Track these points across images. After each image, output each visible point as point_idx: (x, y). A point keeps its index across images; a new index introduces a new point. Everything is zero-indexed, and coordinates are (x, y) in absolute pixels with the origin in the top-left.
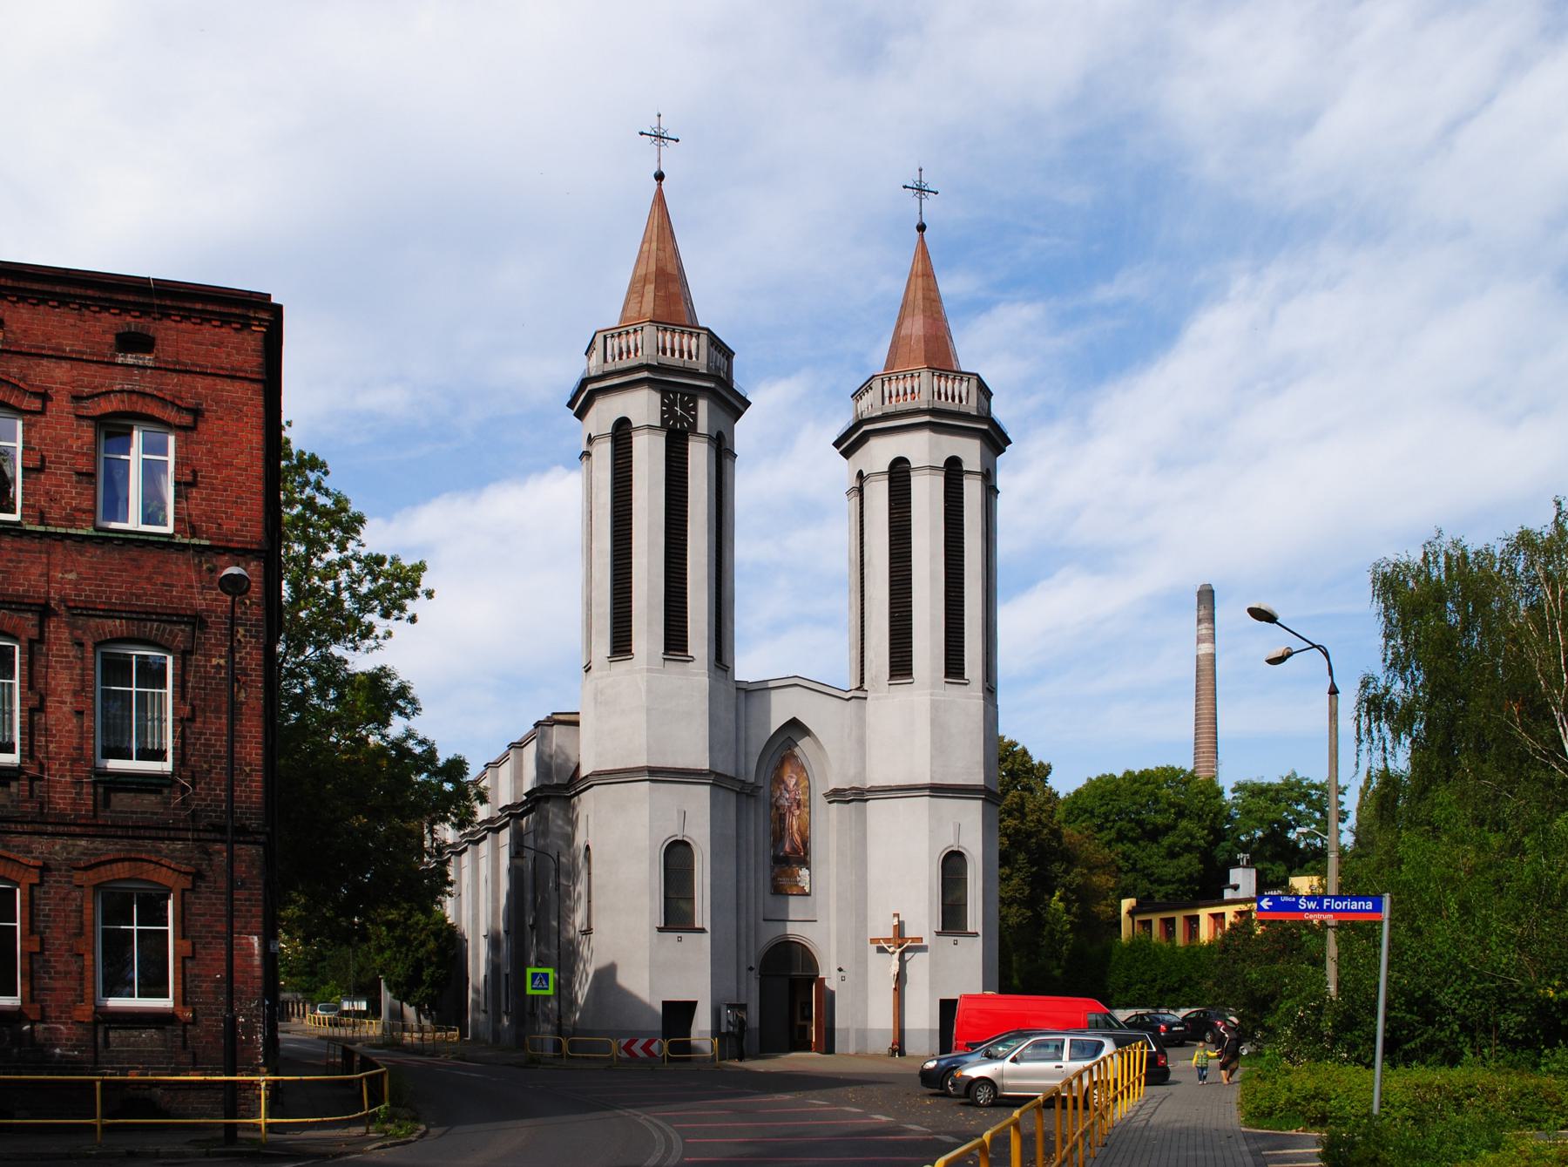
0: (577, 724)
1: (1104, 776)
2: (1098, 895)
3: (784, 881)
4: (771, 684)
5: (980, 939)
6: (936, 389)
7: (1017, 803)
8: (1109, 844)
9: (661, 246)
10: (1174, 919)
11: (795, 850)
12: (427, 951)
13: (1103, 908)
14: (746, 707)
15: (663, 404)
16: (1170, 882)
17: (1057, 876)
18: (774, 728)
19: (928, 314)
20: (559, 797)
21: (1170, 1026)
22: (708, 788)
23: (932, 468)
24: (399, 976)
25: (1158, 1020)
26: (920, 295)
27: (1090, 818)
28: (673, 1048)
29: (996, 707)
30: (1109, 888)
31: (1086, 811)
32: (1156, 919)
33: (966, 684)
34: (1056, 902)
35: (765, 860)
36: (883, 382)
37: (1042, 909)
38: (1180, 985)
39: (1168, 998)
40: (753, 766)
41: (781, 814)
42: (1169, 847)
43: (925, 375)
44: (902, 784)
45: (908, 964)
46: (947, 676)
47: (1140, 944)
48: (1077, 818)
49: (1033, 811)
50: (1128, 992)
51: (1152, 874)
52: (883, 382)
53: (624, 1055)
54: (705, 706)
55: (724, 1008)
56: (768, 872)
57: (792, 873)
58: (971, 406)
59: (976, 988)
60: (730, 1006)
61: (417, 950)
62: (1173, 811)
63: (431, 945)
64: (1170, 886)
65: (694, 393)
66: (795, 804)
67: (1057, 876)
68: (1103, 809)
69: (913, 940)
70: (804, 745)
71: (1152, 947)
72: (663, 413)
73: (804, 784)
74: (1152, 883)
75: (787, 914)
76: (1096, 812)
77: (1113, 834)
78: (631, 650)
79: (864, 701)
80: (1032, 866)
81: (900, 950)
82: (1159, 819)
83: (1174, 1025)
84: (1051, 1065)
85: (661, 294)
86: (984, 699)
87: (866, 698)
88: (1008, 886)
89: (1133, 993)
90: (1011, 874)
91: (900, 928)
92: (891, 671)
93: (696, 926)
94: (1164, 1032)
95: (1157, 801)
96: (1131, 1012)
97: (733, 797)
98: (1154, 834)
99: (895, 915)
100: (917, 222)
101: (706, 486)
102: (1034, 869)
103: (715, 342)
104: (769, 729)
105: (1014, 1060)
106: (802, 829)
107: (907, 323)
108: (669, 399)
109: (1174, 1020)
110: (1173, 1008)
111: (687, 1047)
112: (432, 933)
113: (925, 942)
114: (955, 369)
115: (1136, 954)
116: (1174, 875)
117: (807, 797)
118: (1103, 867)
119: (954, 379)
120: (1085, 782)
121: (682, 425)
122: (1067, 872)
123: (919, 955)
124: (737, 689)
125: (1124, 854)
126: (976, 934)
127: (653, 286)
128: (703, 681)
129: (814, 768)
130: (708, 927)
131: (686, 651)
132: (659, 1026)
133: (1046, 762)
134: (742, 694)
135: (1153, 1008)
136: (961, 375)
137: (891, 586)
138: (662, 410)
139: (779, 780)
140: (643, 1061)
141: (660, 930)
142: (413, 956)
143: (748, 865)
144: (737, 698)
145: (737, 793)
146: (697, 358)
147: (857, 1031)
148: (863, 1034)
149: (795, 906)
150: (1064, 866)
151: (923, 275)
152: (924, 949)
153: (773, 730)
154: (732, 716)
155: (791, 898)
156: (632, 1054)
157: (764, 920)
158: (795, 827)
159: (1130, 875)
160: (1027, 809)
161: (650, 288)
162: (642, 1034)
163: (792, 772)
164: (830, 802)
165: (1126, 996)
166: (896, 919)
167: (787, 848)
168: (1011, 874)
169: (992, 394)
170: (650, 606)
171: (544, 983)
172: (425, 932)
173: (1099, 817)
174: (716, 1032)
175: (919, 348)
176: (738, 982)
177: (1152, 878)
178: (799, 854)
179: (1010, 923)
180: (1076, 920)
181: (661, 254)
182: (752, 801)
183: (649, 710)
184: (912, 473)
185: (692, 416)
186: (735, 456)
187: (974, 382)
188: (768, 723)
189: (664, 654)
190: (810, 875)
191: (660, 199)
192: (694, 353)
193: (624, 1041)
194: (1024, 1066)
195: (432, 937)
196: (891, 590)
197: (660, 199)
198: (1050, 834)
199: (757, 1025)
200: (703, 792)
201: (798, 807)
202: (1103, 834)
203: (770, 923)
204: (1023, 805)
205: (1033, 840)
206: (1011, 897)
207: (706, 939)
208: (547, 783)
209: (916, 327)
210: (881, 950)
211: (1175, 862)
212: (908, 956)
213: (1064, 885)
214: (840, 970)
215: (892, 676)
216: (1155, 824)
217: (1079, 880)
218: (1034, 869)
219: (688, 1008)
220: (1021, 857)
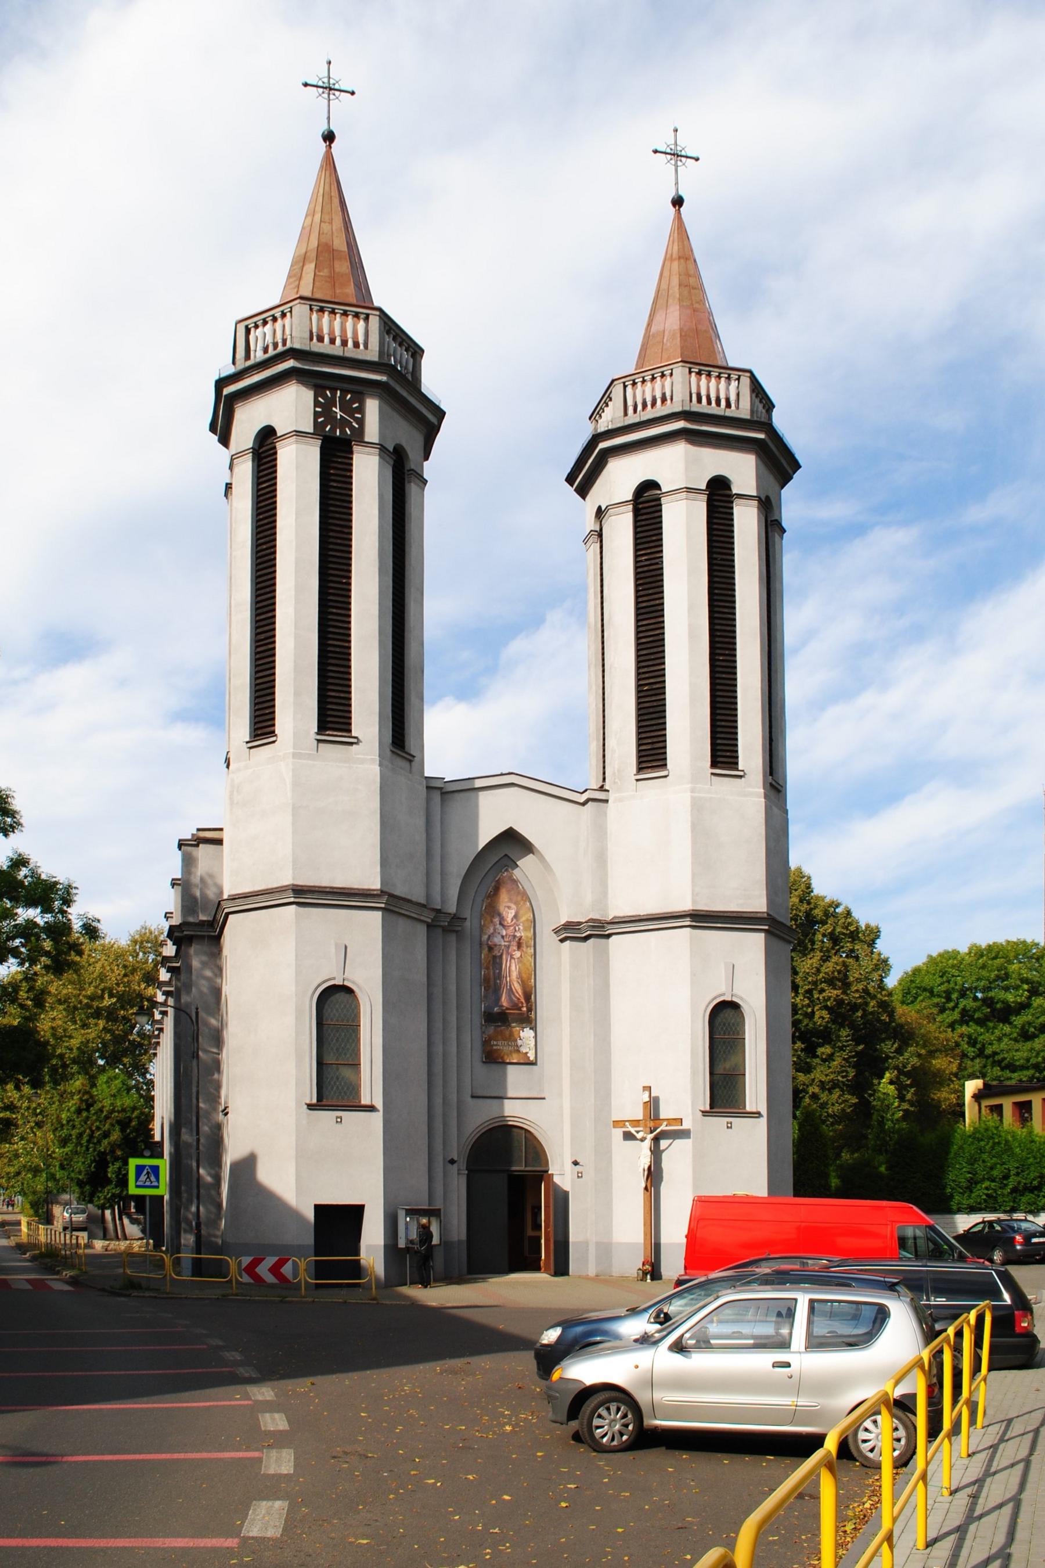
0: (219, 842)
1: (947, 952)
2: (938, 1079)
3: (499, 1045)
4: (478, 784)
5: (763, 1122)
6: (694, 390)
7: (839, 972)
8: (952, 1026)
9: (327, 218)
10: (1030, 1103)
11: (516, 1006)
12: (109, 1143)
13: (944, 1095)
14: (443, 812)
15: (317, 404)
16: (1023, 1068)
17: (888, 1057)
18: (484, 839)
19: (686, 303)
20: (202, 937)
21: (1028, 1236)
22: (378, 915)
23: (689, 490)
24: (80, 1172)
25: (1012, 1228)
26: (675, 281)
27: (930, 998)
28: (321, 1270)
29: (786, 812)
30: (951, 1073)
31: (925, 990)
32: (1007, 1104)
33: (740, 777)
34: (886, 1086)
35: (473, 1018)
36: (625, 387)
37: (871, 1095)
38: (1040, 1183)
39: (1024, 1199)
40: (454, 892)
41: (495, 957)
42: (1023, 1027)
43: (680, 371)
44: (654, 912)
45: (664, 1156)
46: (714, 764)
47: (987, 1130)
48: (916, 998)
49: (858, 980)
50: (971, 1192)
51: (1004, 1059)
52: (625, 387)
53: (246, 1279)
54: (375, 803)
55: (401, 1214)
56: (477, 1033)
57: (511, 1034)
58: (744, 409)
59: (759, 1188)
60: (410, 1212)
61: (99, 1142)
62: (1026, 987)
63: (116, 1136)
64: (1026, 1073)
65: (360, 389)
66: (514, 943)
67: (888, 1057)
68: (943, 988)
69: (670, 1121)
70: (526, 864)
71: (1003, 1134)
72: (316, 415)
73: (526, 916)
74: (1002, 1069)
75: (504, 1087)
76: (935, 990)
77: (956, 1015)
78: (274, 732)
79: (605, 804)
80: (858, 1044)
81: (652, 1135)
82: (1010, 997)
83: (1034, 1235)
84: (762, 1361)
85: (325, 272)
86: (766, 796)
87: (607, 801)
88: (830, 1067)
89: (980, 1191)
90: (833, 1054)
91: (653, 1106)
92: (639, 763)
93: (363, 1102)
94: (1021, 1244)
95: (1007, 976)
96: (976, 1218)
97: (422, 930)
98: (1005, 1013)
99: (645, 1088)
100: (672, 194)
101: (376, 512)
102: (861, 1047)
103: (390, 328)
104: (476, 844)
105: (679, 1347)
106: (524, 976)
107: (659, 317)
108: (325, 397)
109: (1033, 1228)
110: (1031, 1212)
111: (356, 1269)
112: (119, 1122)
113: (686, 1125)
114: (720, 363)
115: (982, 1143)
116: (1028, 1060)
117: (530, 934)
118: (949, 1050)
119: (719, 377)
120: (925, 960)
121: (343, 431)
122: (899, 1051)
123: (678, 1142)
124: (428, 788)
125: (969, 1037)
126: (758, 1115)
127: (313, 265)
128: (373, 770)
129: (539, 895)
130: (379, 1103)
131: (350, 731)
132: (309, 1239)
133: (873, 924)
134: (437, 797)
135: (1005, 1212)
136: (727, 372)
137: (638, 650)
138: (315, 412)
139: (492, 910)
140: (272, 1286)
141: (311, 1107)
142: (95, 1150)
143: (445, 1021)
144: (428, 800)
145: (429, 926)
146: (366, 347)
147: (598, 1244)
148: (606, 1249)
149: (515, 1078)
150: (896, 1045)
151: (679, 258)
152: (685, 1134)
153: (481, 847)
154: (421, 822)
155: (510, 1067)
156: (258, 1279)
157: (473, 1097)
158: (514, 974)
159: (977, 1061)
160: (851, 979)
161: (310, 267)
162: (272, 1249)
163: (511, 900)
164: (562, 941)
165: (969, 1197)
166: (647, 1094)
167: (504, 1001)
168: (833, 1054)
169: (774, 407)
170: (297, 669)
171: (153, 1178)
172: (109, 1121)
173: (939, 996)
174: (391, 1248)
175: (674, 349)
176: (431, 1179)
177: (1003, 1064)
178: (520, 1009)
179: (830, 1111)
180: (912, 1109)
181: (326, 227)
182: (453, 938)
183: (296, 810)
184: (663, 500)
185: (357, 420)
186: (425, 482)
187: (746, 381)
188: (475, 835)
189: (318, 734)
190: (536, 1037)
191: (329, 163)
192: (361, 340)
193: (246, 1260)
194: (700, 1362)
195: (117, 1128)
196: (638, 656)
197: (329, 163)
198: (879, 1007)
199: (463, 1236)
200: (372, 921)
201: (519, 946)
202: (945, 1015)
203: (480, 1101)
204: (846, 977)
205: (859, 1014)
206: (832, 1080)
207: (376, 1120)
208: (191, 919)
209: (672, 320)
210: (628, 1136)
211: (1029, 1044)
212: (664, 1144)
213: (896, 1068)
214: (576, 1163)
215: (640, 769)
216: (1005, 1002)
217: (915, 1061)
218: (861, 1047)
219: (354, 1214)
220: (844, 1033)
